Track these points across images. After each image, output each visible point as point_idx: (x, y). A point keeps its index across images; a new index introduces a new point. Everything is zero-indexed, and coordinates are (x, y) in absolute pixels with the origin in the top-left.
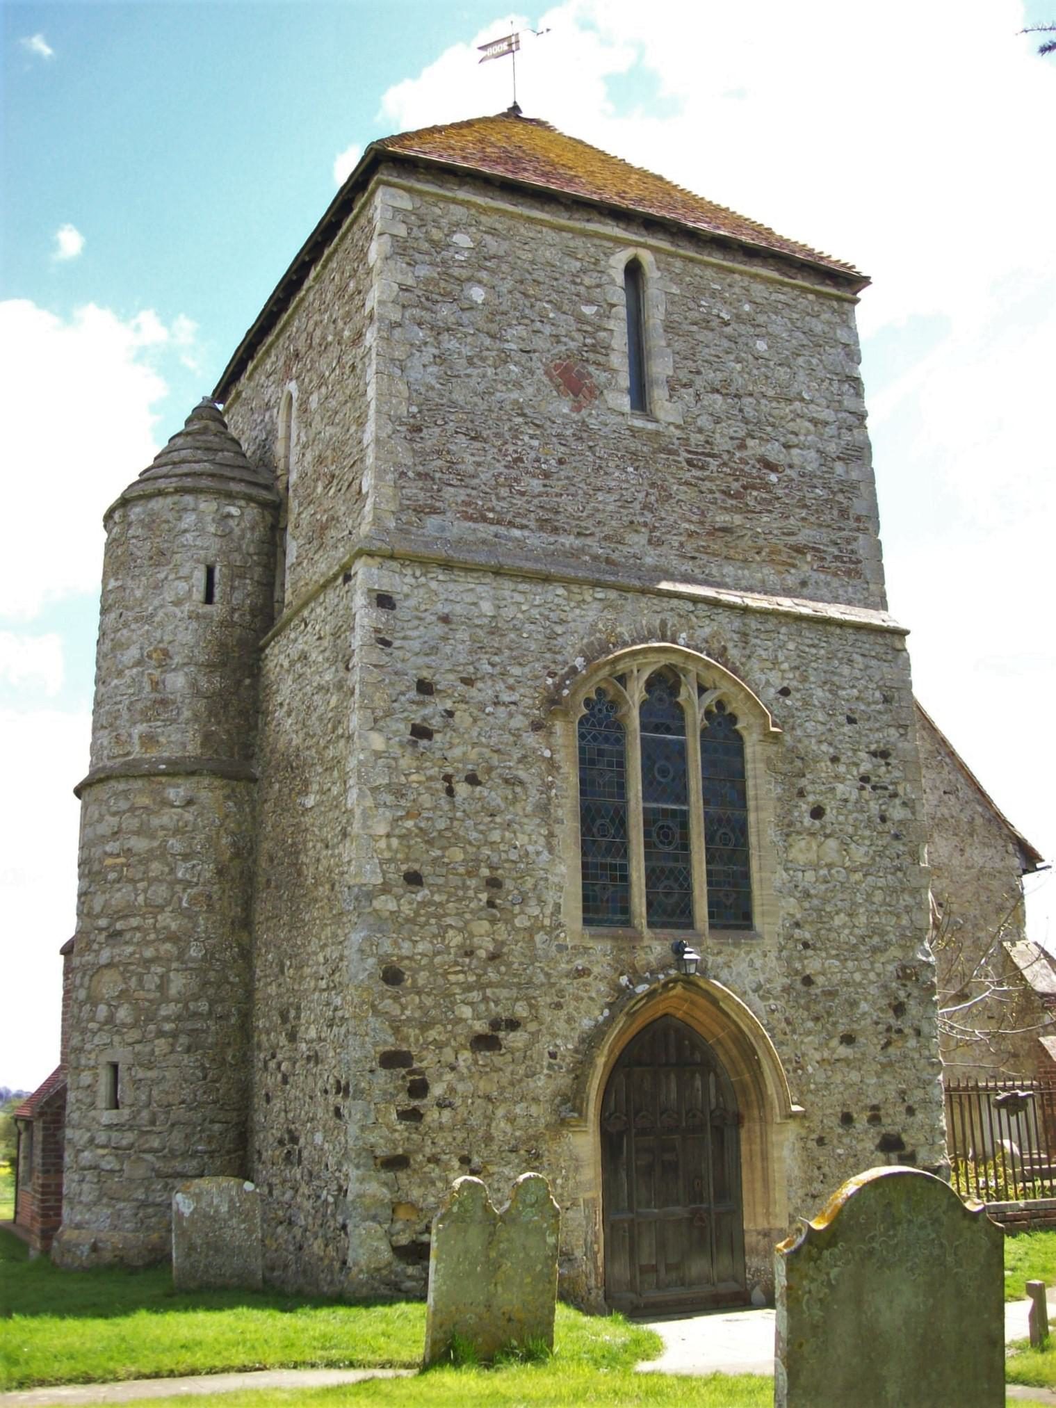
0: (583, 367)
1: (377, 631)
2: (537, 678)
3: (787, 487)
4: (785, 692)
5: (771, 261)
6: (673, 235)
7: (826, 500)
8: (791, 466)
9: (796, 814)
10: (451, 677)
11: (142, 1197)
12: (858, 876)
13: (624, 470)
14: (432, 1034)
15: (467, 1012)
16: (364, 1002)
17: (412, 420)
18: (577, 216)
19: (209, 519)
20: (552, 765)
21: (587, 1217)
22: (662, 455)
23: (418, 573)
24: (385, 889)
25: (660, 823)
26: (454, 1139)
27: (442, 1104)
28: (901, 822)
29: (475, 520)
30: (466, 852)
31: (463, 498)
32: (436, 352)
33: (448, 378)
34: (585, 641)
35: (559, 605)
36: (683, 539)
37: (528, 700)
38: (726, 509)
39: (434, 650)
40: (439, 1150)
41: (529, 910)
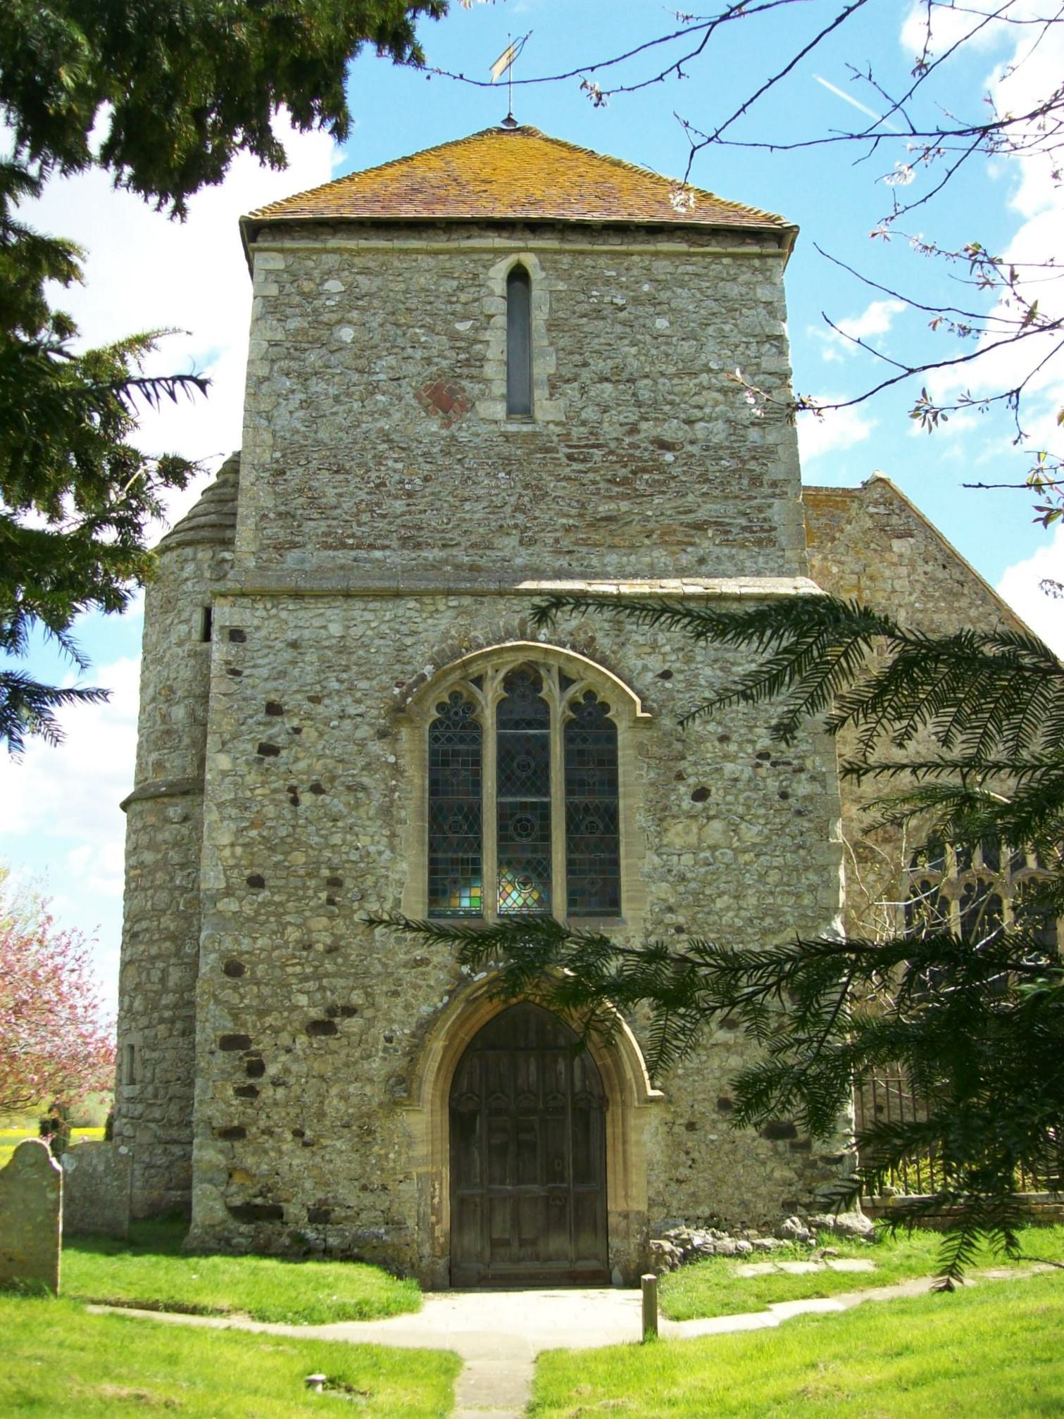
0: (456, 383)
1: (228, 663)
2: (385, 689)
3: (685, 464)
4: (666, 675)
5: (679, 233)
6: (562, 231)
7: (734, 471)
8: (692, 442)
9: (673, 798)
10: (299, 697)
11: (147, 1160)
12: (747, 857)
13: (495, 477)
14: (269, 1020)
15: (303, 1000)
16: (204, 992)
17: (275, 466)
18: (454, 236)
19: (206, 566)
20: (396, 770)
21: (420, 1190)
22: (539, 456)
23: (269, 606)
24: (229, 892)
25: (518, 817)
26: (288, 1114)
27: (276, 1083)
28: (805, 798)
29: (335, 549)
30: (308, 856)
31: (323, 529)
32: (303, 396)
33: (312, 422)
34: (436, 648)
35: (410, 618)
36: (558, 534)
37: (375, 710)
38: (610, 497)
39: (282, 674)
40: (272, 1123)
41: (368, 906)
